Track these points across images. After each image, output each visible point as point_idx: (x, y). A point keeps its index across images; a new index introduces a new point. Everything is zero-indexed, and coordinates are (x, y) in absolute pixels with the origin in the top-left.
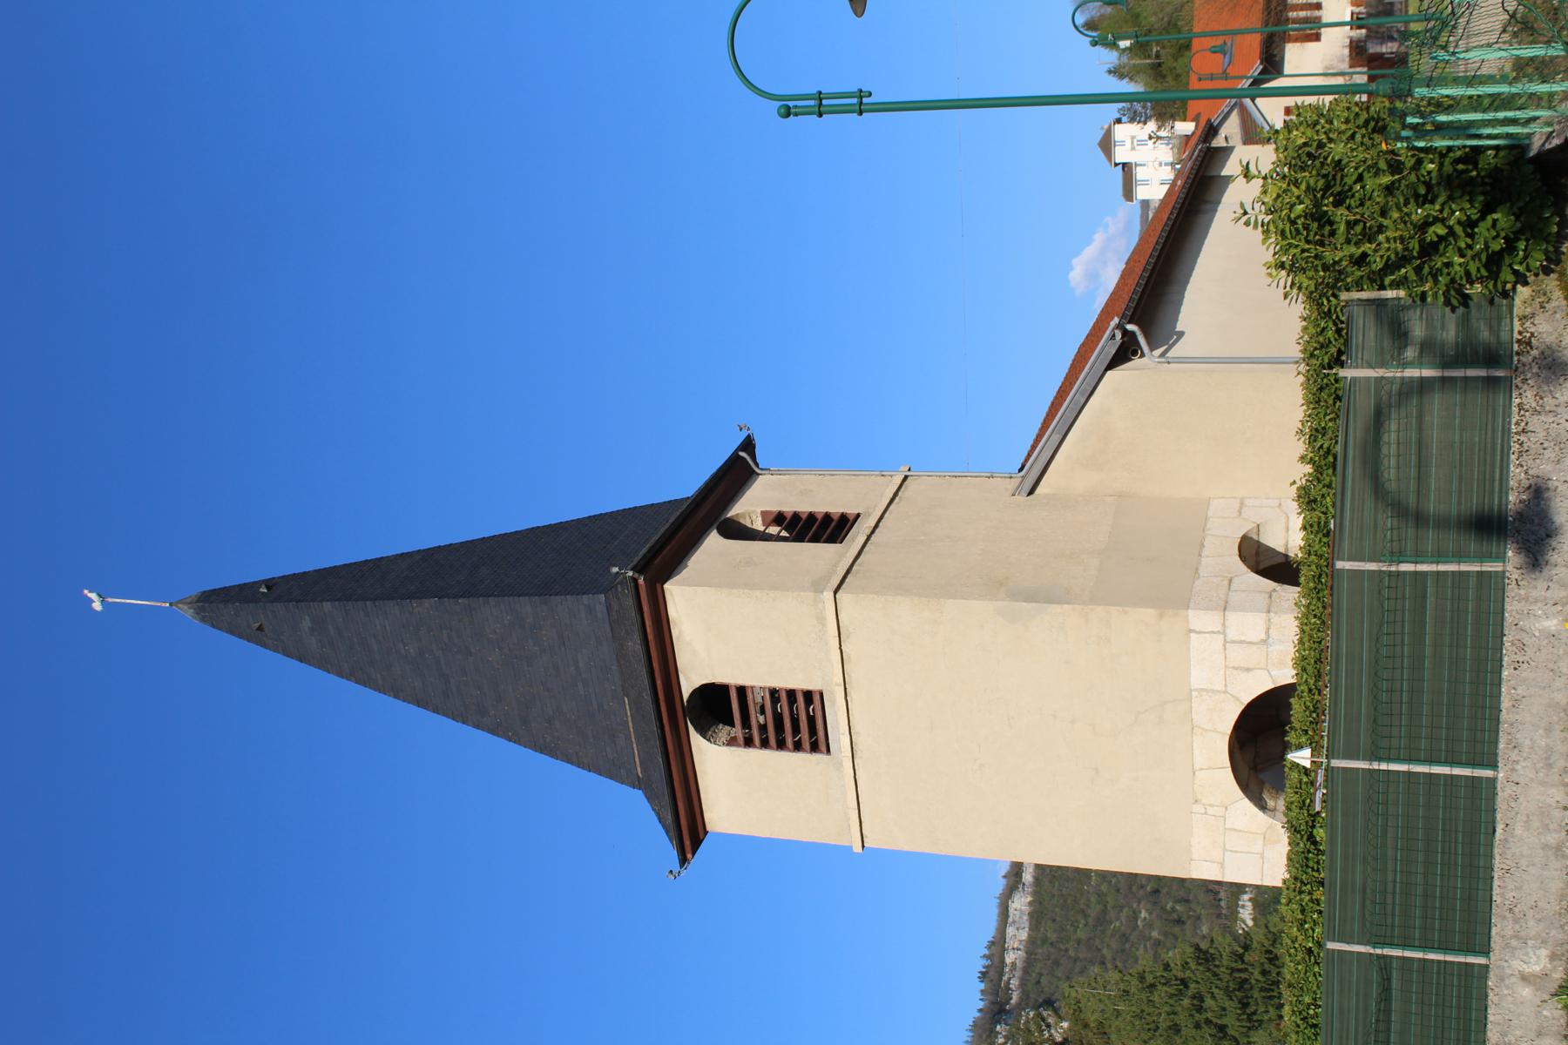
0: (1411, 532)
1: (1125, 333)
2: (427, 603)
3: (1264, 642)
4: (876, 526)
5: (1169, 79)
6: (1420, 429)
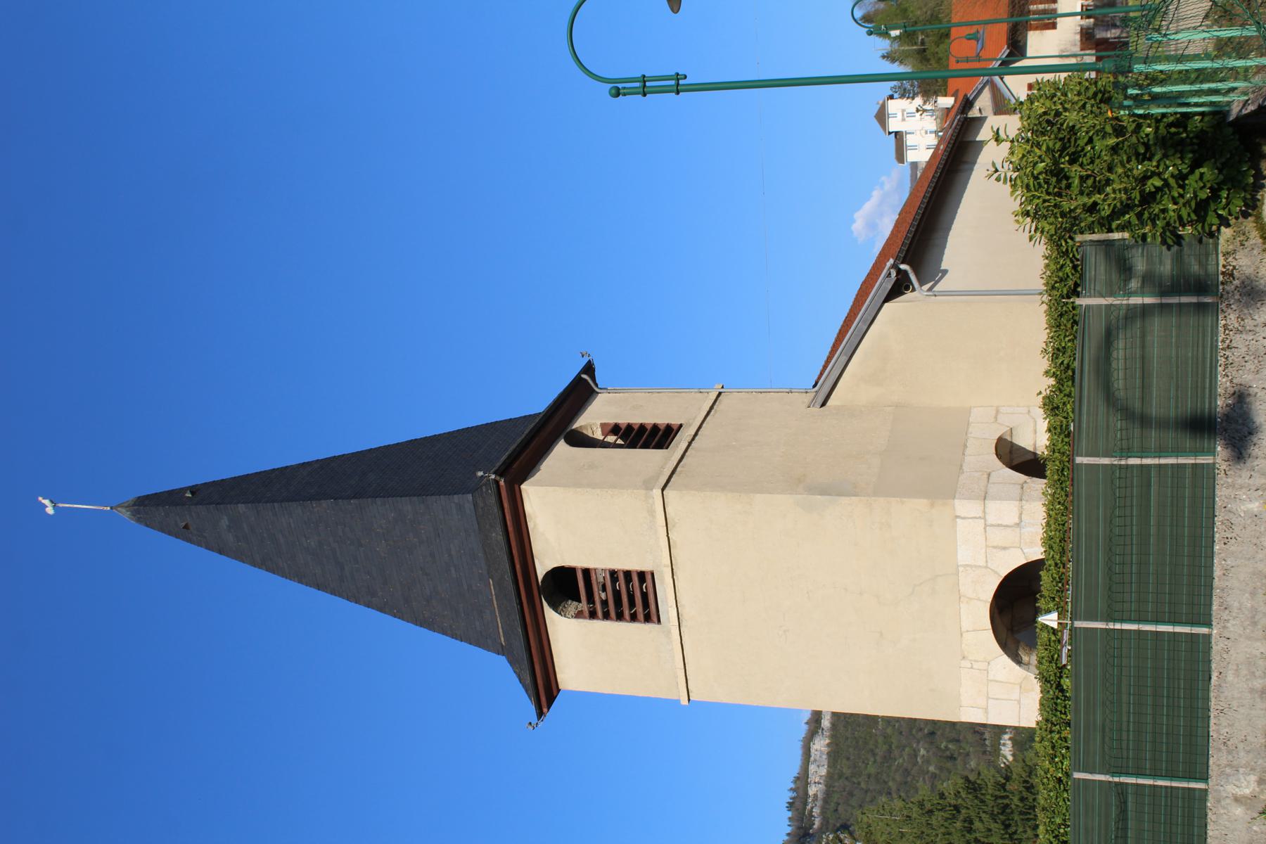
0: (1137, 431)
1: (899, 271)
2: (324, 503)
3: (1018, 525)
4: (696, 434)
5: (933, 62)
6: (1143, 347)
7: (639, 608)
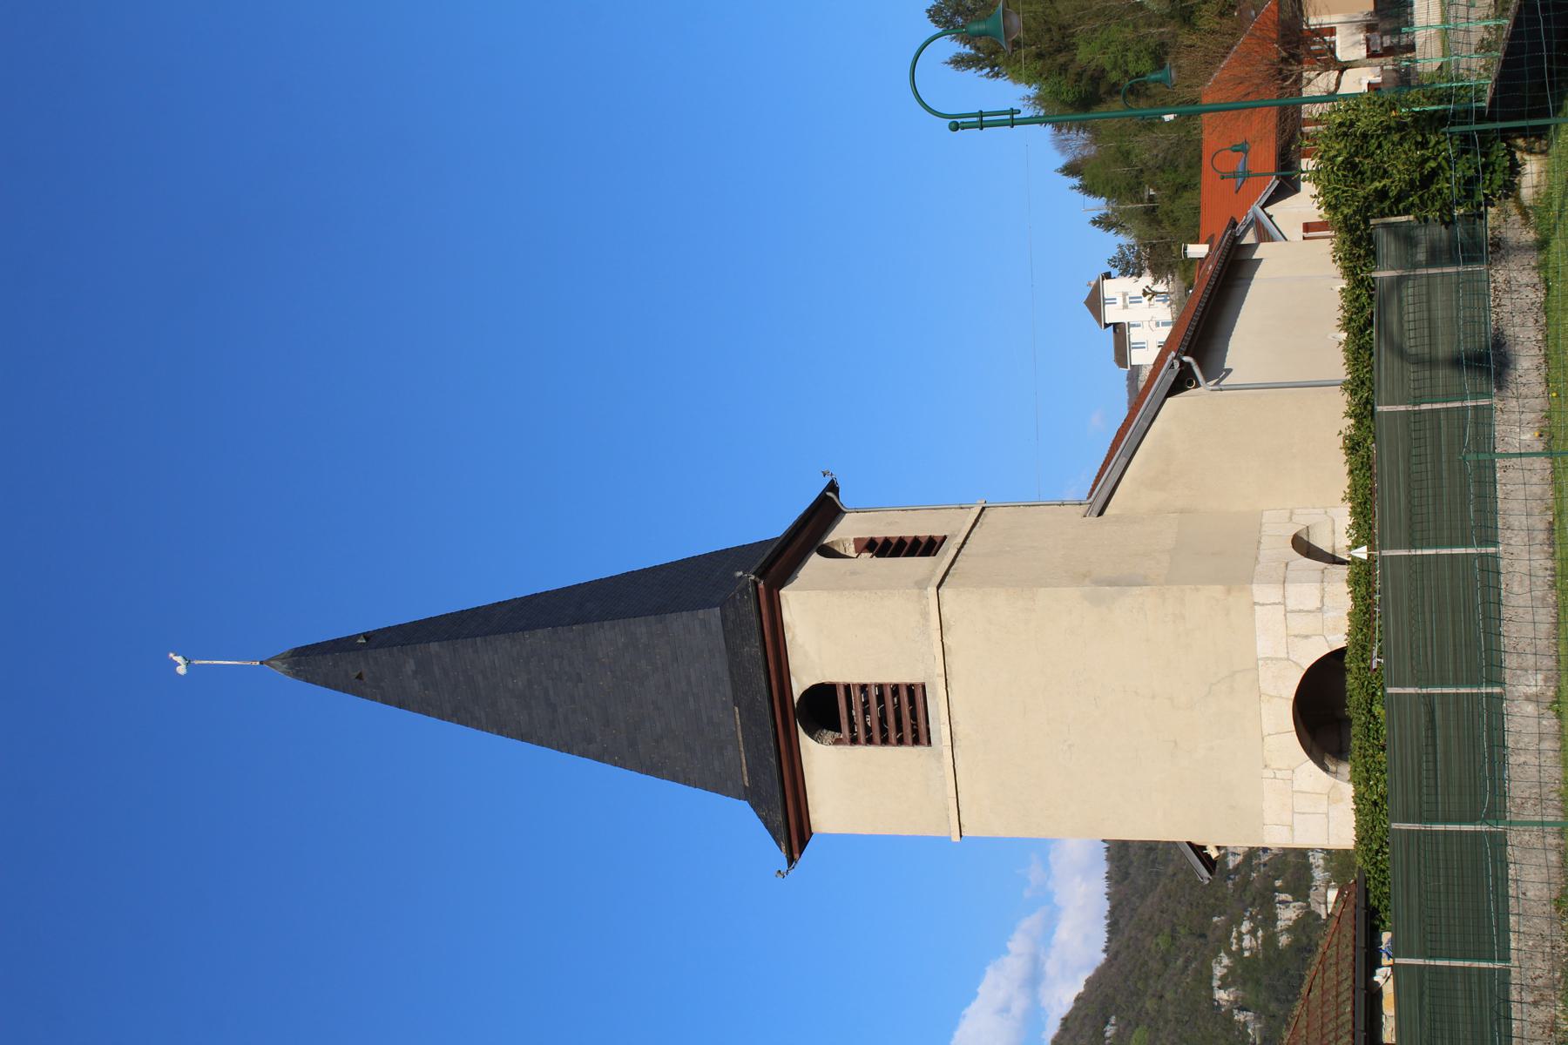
0: (1427, 373)
1: (1182, 363)
2: (539, 632)
3: (1320, 609)
4: (964, 543)
5: (1166, 224)
6: (1429, 310)
7: (907, 729)
